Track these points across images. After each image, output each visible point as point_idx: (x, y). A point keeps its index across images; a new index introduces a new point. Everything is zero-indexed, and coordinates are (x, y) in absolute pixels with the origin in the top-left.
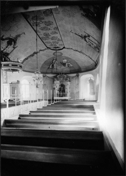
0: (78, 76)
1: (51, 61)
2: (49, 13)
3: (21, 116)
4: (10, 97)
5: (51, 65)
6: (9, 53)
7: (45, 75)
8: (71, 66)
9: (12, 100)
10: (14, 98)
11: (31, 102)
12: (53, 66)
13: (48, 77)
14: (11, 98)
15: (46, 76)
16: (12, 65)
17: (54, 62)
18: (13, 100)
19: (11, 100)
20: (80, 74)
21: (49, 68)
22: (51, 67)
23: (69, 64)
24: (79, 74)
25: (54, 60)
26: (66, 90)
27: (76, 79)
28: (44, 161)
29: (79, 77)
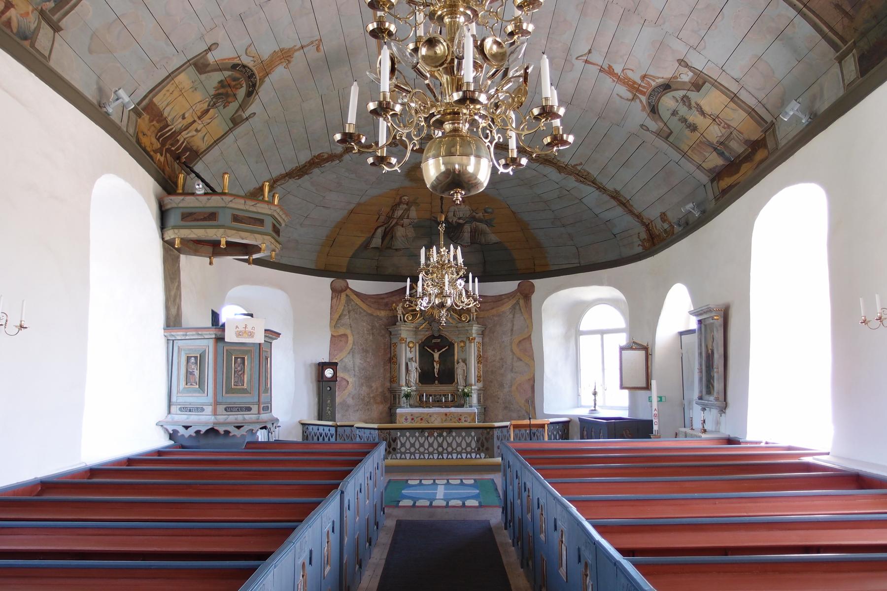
0: (526, 294)
1: (386, 210)
2: (460, 34)
3: (622, 387)
4: (215, 413)
5: (380, 231)
6: (203, 146)
7: (340, 283)
8: (493, 238)
9: (227, 433)
10: (239, 417)
11: (412, 417)
12: (388, 234)
13: (357, 294)
14: (221, 418)
15: (347, 287)
16: (236, 219)
17: (401, 217)
18: (234, 431)
19: (221, 430)
20: (539, 283)
21: (366, 246)
22: (377, 242)
23: (483, 233)
24: (533, 286)
25: (400, 203)
26: (459, 370)
27: (513, 308)
28: (717, 503)
29: (534, 297)
